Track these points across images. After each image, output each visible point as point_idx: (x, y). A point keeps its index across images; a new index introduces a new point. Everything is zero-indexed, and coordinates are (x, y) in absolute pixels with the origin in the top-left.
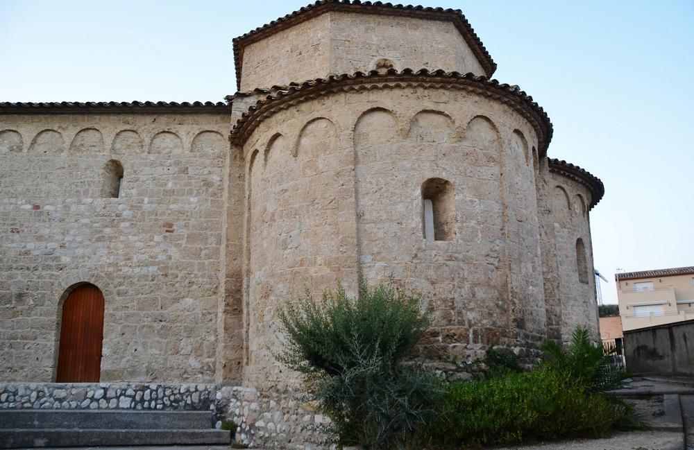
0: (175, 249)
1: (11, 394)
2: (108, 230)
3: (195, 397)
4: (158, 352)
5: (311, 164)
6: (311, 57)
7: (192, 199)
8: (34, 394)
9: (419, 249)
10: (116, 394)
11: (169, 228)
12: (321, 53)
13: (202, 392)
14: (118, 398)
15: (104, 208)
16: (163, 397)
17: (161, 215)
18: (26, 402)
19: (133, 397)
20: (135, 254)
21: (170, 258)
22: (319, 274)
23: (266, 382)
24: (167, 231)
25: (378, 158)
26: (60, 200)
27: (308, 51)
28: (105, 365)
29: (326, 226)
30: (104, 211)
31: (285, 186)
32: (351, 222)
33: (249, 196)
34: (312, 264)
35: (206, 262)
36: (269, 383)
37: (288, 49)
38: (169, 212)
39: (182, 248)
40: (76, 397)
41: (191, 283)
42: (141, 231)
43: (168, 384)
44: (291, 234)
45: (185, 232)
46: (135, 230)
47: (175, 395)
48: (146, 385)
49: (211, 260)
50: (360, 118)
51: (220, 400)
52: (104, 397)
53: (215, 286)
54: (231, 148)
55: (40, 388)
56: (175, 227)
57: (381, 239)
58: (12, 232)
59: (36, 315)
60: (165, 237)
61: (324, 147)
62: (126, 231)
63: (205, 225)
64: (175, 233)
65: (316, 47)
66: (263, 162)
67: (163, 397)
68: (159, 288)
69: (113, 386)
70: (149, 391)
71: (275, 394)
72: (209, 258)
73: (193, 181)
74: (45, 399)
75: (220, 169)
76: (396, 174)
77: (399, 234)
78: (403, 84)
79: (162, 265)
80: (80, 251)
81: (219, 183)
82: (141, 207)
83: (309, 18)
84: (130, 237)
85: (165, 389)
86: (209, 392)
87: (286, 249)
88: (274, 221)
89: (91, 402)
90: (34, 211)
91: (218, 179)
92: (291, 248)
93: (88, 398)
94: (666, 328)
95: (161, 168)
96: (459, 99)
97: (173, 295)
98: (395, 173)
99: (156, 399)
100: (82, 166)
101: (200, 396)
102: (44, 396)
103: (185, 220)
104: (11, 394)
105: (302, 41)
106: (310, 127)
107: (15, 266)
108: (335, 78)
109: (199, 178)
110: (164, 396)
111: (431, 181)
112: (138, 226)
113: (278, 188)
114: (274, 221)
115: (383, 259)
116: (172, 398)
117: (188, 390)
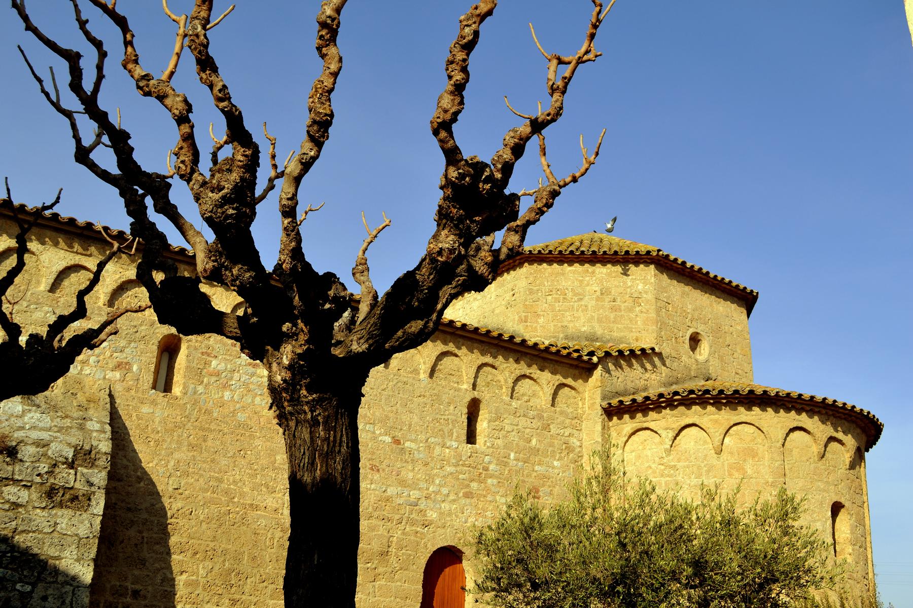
2: (474, 485)
6: (631, 310)
7: (556, 463)
12: (644, 310)
17: (527, 476)
26: (422, 437)
27: (625, 302)
38: (535, 474)
46: (502, 491)
50: (787, 435)
56: (541, 494)
58: (372, 469)
59: (400, 580)
62: (493, 489)
73: (556, 442)
76: (815, 493)
78: (824, 412)
80: (445, 506)
81: (579, 449)
90: (394, 446)
91: (578, 444)
95: (523, 419)
96: (851, 431)
100: (445, 398)
106: (735, 428)
107: (376, 514)
108: (781, 394)
111: (840, 503)
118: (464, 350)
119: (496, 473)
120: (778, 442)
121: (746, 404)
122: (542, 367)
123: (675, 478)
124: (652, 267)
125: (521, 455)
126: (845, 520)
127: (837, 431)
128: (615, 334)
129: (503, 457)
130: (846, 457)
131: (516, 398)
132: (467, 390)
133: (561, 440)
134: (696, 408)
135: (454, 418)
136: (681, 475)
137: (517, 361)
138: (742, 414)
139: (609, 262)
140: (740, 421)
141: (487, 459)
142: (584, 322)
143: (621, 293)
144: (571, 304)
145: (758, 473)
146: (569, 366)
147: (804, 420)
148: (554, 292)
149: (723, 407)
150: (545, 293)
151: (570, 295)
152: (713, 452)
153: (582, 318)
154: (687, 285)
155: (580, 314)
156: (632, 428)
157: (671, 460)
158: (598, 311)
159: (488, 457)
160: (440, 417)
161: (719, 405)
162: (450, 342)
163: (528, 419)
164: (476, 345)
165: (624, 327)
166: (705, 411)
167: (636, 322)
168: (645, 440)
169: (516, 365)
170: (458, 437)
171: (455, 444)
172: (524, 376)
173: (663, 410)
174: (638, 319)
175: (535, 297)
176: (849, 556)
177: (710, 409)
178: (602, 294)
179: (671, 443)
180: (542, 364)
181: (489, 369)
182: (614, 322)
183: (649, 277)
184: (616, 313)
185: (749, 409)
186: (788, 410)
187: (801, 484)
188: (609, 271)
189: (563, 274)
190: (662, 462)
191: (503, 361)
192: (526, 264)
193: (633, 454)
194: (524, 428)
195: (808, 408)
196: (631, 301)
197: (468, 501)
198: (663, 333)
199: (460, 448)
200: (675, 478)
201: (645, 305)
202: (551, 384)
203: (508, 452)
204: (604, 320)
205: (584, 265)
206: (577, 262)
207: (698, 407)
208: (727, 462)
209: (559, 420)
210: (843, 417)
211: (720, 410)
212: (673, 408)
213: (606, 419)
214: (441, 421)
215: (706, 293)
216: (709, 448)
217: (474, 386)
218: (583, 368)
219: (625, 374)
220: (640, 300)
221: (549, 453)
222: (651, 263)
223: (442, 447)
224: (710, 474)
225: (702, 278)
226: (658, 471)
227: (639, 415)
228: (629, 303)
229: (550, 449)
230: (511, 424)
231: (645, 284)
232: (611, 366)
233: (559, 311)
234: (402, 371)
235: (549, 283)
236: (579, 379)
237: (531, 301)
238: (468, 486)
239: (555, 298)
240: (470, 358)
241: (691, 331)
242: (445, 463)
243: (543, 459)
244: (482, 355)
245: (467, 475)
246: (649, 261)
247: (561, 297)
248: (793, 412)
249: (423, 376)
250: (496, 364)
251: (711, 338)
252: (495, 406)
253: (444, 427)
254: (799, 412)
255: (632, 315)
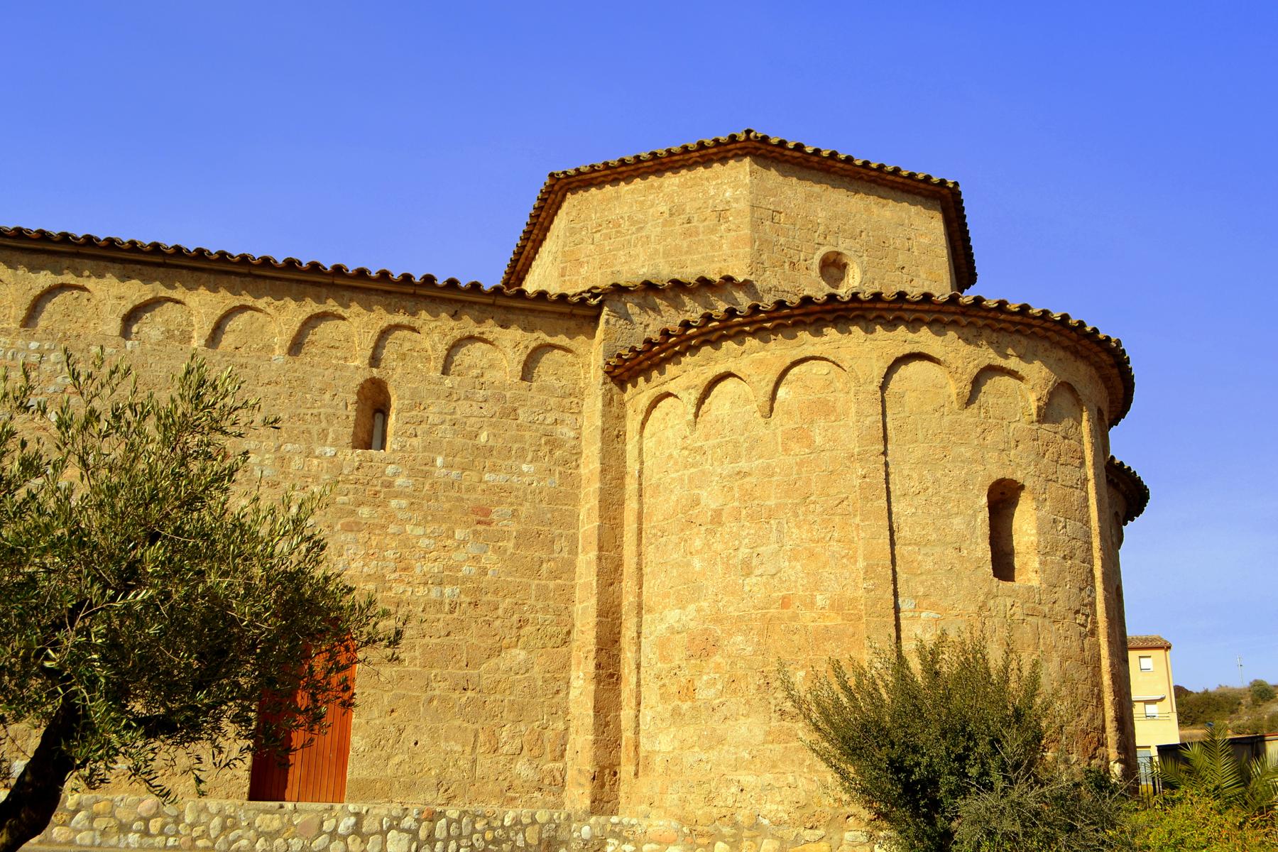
0: (495, 557)
1: (170, 820)
2: (364, 512)
3: (532, 835)
4: (458, 748)
5: (801, 435)
6: (713, 231)
7: (525, 467)
8: (216, 821)
9: (987, 594)
10: (382, 826)
11: (483, 516)
12: (733, 227)
13: (543, 825)
14: (384, 833)
15: (358, 468)
16: (472, 834)
17: (468, 490)
18: (199, 837)
19: (414, 834)
20: (417, 560)
21: (484, 572)
22: (821, 623)
23: (707, 809)
24: (479, 522)
25: (920, 436)
28: (355, 770)
29: (831, 543)
30: (359, 475)
31: (743, 465)
32: (880, 541)
33: (641, 472)
34: (805, 605)
35: (552, 584)
36: (715, 810)
37: (665, 209)
38: (483, 486)
39: (506, 557)
40: (301, 831)
41: (522, 623)
42: (430, 518)
43: (476, 807)
44: (760, 550)
45: (513, 527)
46: (417, 516)
47: (494, 829)
48: (439, 809)
49: (559, 581)
51: (587, 841)
52: (357, 830)
53: (565, 631)
54: (604, 383)
55: (229, 810)
56: (494, 516)
57: (929, 572)
60: (475, 532)
61: (825, 409)
63: (549, 516)
64: (493, 527)
65: (721, 215)
66: (691, 417)
67: (472, 834)
68: (462, 626)
69: (374, 812)
70: (444, 821)
71: (727, 830)
72: (556, 578)
73: (527, 434)
74: (239, 832)
75: (575, 416)
76: (949, 466)
77: (958, 566)
78: (964, 321)
79: (469, 585)
82: (431, 473)
83: (707, 162)
84: (409, 528)
85: (475, 817)
86: (558, 826)
87: (748, 575)
88: (720, 524)
89: (330, 842)
91: (572, 434)
92: (761, 575)
93: (325, 832)
94: (1247, 744)
97: (490, 642)
98: (949, 466)
99: (459, 837)
100: (316, 383)
101: (540, 832)
102: (235, 826)
103: (511, 504)
104: (170, 820)
105: (693, 200)
106: (795, 370)
108: (861, 296)
109: (537, 430)
110: (474, 831)
111: (1013, 482)
112: (425, 508)
113: (728, 468)
114: (720, 524)
115: (932, 606)
116: (489, 836)
117: (517, 821)
118: (355, 308)
119: (407, 490)
120: (872, 382)
121: (811, 324)
122: (503, 321)
123: (701, 468)
124: (747, 160)
125: (458, 459)
126: (1028, 511)
127: (1006, 357)
128: (689, 270)
129: (420, 465)
130: (1031, 400)
131: (456, 373)
132: (357, 368)
133: (537, 430)
134: (728, 345)
135: (330, 411)
136: (709, 461)
137: (455, 316)
138: (807, 343)
139: (683, 167)
140: (802, 356)
141: (390, 469)
142: (644, 262)
143: (700, 208)
144: (629, 237)
145: (835, 441)
146: (556, 316)
147: (925, 339)
148: (604, 225)
149: (773, 337)
150: (592, 229)
151: (625, 225)
152: (758, 415)
153: (641, 256)
154: (819, 182)
155: (639, 249)
156: (649, 398)
157: (697, 439)
158: (665, 240)
159: (393, 466)
160: (306, 411)
161: (763, 334)
162: (327, 298)
163: (474, 404)
164: (374, 298)
165: (703, 258)
166: (743, 348)
167: (721, 247)
168: (667, 414)
169: (453, 323)
170: (336, 439)
171: (330, 451)
172: (471, 339)
173: (682, 359)
174: (723, 241)
175: (577, 238)
176: (1034, 574)
177: (751, 342)
178: (671, 215)
179: (694, 411)
180: (503, 317)
181: (406, 333)
182: (687, 253)
183: (742, 177)
184: (691, 239)
185: (818, 333)
186: (891, 325)
187: (918, 454)
188: (682, 180)
189: (618, 198)
190: (685, 445)
191: (429, 317)
192: (569, 195)
193: (654, 439)
194: (465, 417)
195: (928, 318)
196: (713, 217)
197: (350, 536)
198: (764, 257)
199: (340, 455)
200: (701, 468)
201: (735, 219)
202: (522, 347)
203: (432, 455)
204: (673, 252)
205: (647, 178)
206: (638, 176)
207: (730, 342)
208: (781, 429)
209: (535, 400)
210: (1013, 329)
211: (767, 341)
212: (694, 351)
213: (616, 389)
214: (307, 417)
215: (857, 192)
216: (753, 409)
217: (375, 361)
218: (584, 317)
219: (664, 319)
220: (728, 213)
221: (513, 452)
222: (745, 155)
223: (307, 457)
224: (754, 453)
225: (845, 170)
226: (680, 460)
227: (655, 374)
228: (712, 221)
229: (515, 446)
230: (441, 413)
231: (735, 188)
232: (632, 308)
233: (610, 251)
234: (242, 350)
235: (598, 215)
236: (578, 334)
237: (572, 244)
238: (353, 512)
239: (606, 234)
240: (366, 318)
241: (823, 251)
242: (310, 480)
243: (499, 462)
244: (389, 312)
245: (351, 496)
246: (740, 152)
247: (614, 230)
248: (902, 328)
249: (279, 355)
250: (417, 323)
251: (865, 258)
252: (410, 388)
253: (310, 426)
254: (914, 325)
255: (715, 238)
